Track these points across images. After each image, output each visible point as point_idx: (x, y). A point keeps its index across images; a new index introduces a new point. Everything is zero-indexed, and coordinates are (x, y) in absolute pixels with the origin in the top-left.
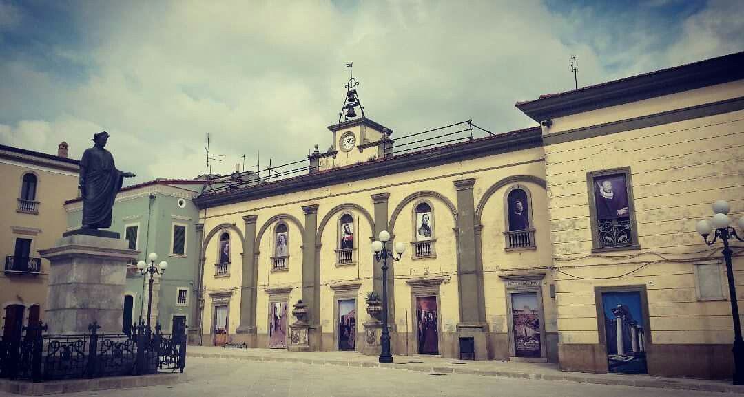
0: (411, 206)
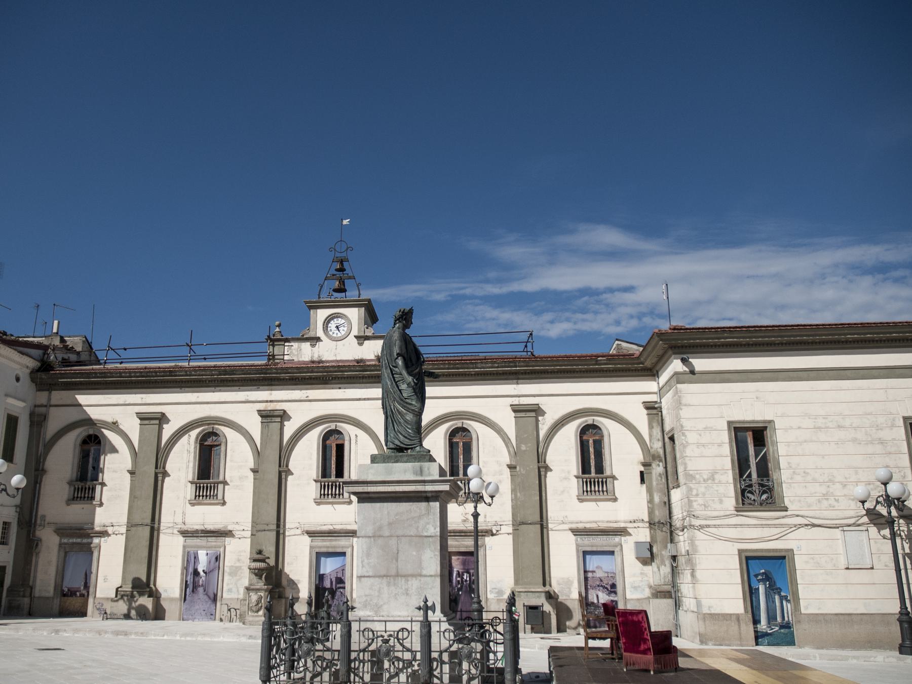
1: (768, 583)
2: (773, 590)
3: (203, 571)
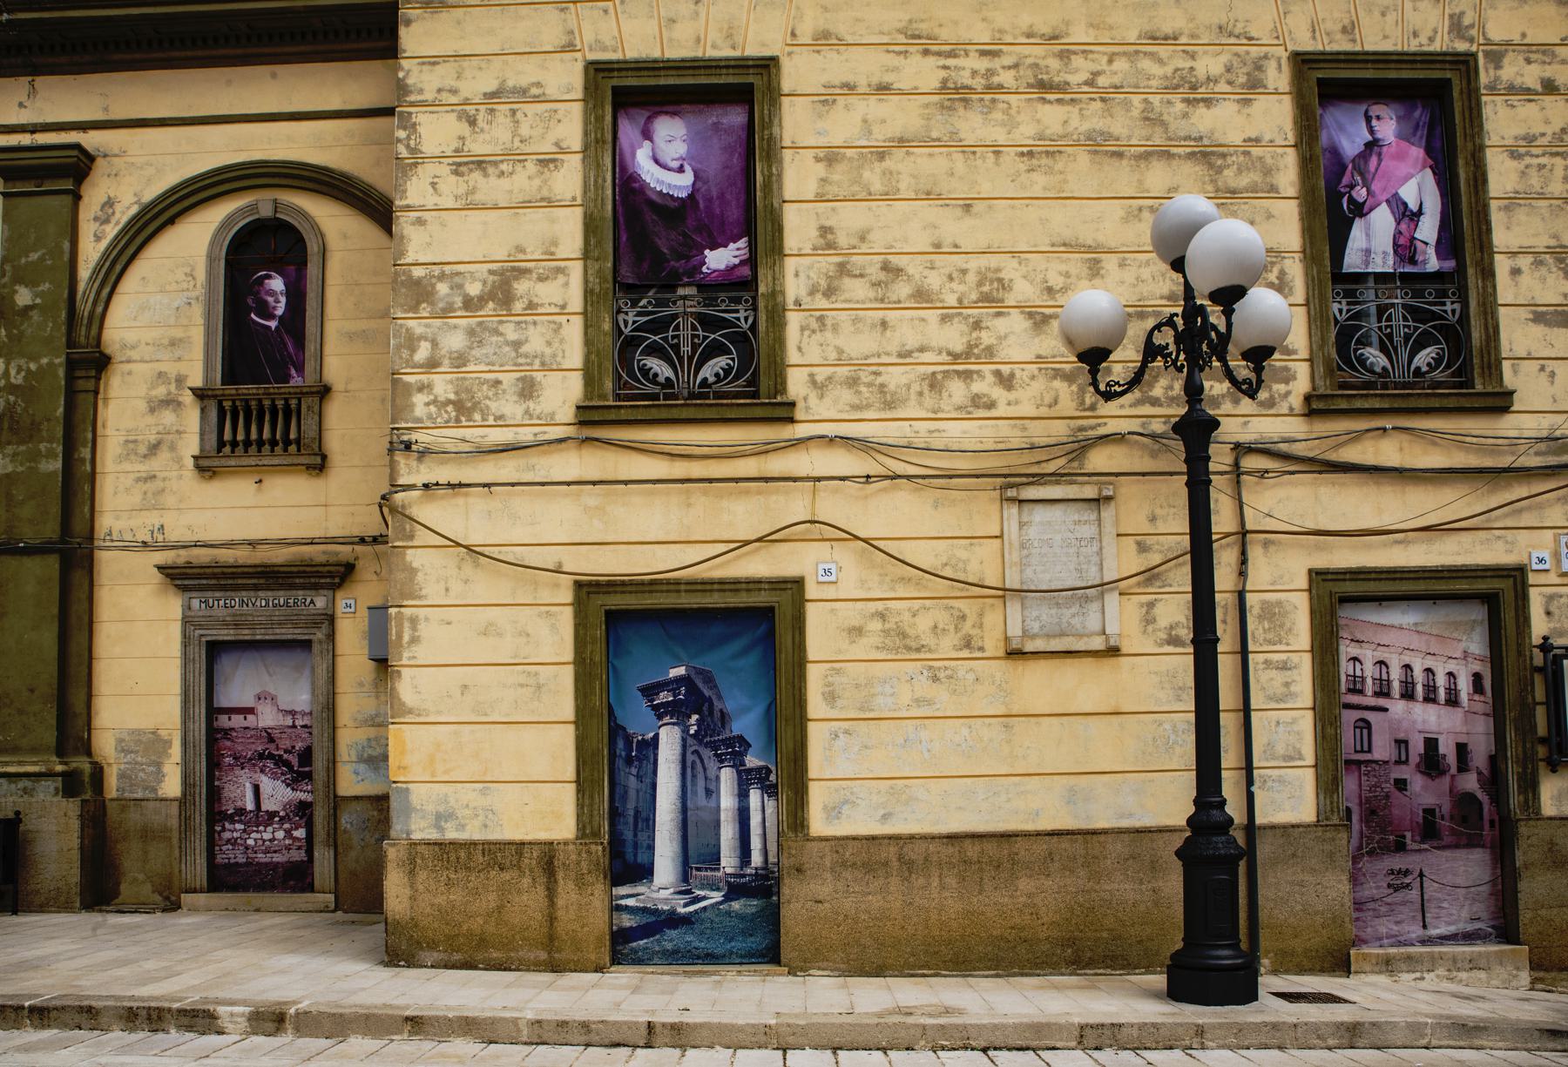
1: (695, 717)
2: (714, 746)
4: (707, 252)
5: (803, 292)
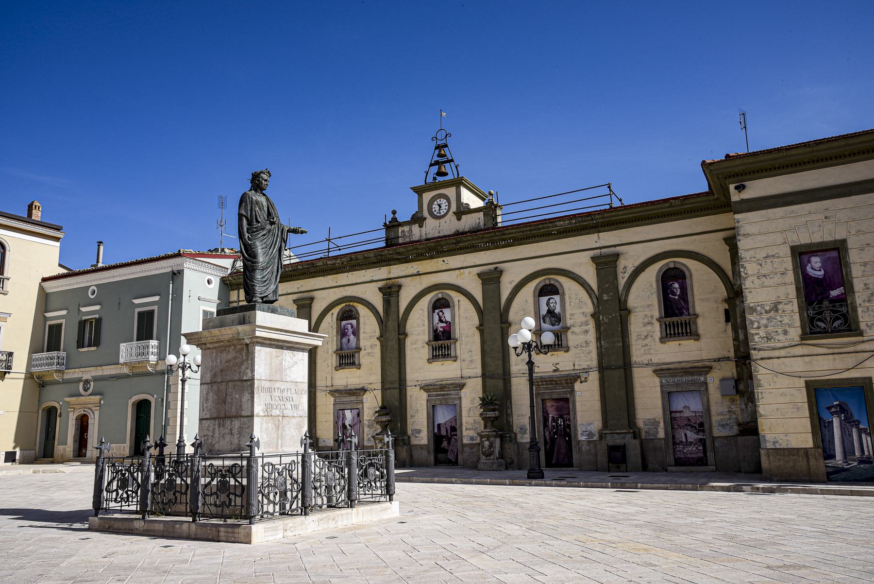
0: (425, 302)
3: (349, 425)
4: (831, 292)
5: (861, 302)
